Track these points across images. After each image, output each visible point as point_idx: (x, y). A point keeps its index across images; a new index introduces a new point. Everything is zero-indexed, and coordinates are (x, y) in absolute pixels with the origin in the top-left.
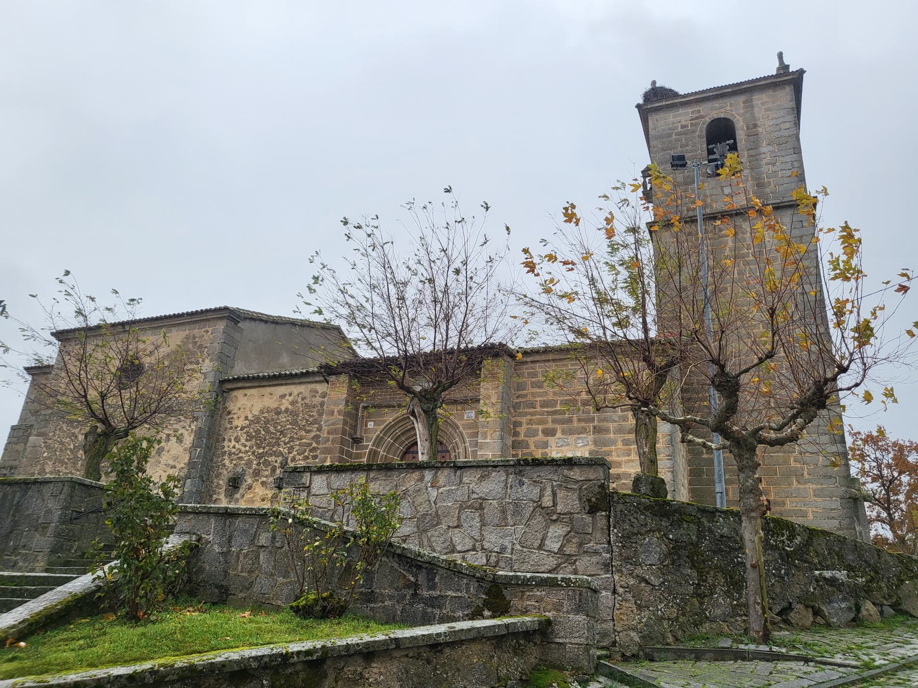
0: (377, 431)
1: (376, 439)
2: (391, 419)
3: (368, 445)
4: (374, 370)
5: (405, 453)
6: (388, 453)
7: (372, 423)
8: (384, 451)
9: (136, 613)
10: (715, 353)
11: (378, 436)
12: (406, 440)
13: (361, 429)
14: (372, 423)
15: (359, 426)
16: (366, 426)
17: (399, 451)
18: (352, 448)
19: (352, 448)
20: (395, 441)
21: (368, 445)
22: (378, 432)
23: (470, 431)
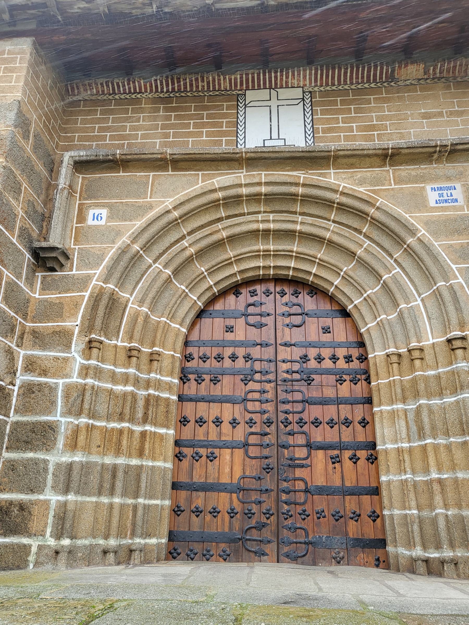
0: (119, 233)
1: (117, 260)
2: (169, 203)
3: (89, 278)
4: (458, 176)
5: (201, 314)
6: (152, 308)
7: (104, 212)
8: (141, 302)
9: (382, 512)
10: (301, 100)
11: (124, 251)
12: (211, 272)
13: (64, 228)
14: (104, 212)
15: (58, 216)
16: (81, 218)
17: (187, 305)
18: (30, 281)
19: (30, 281)
20: (176, 272)
21: (87, 279)
22: (125, 239)
23: (456, 241)
